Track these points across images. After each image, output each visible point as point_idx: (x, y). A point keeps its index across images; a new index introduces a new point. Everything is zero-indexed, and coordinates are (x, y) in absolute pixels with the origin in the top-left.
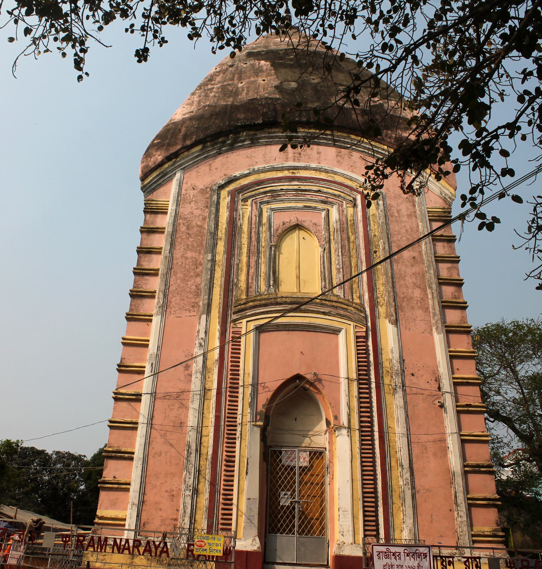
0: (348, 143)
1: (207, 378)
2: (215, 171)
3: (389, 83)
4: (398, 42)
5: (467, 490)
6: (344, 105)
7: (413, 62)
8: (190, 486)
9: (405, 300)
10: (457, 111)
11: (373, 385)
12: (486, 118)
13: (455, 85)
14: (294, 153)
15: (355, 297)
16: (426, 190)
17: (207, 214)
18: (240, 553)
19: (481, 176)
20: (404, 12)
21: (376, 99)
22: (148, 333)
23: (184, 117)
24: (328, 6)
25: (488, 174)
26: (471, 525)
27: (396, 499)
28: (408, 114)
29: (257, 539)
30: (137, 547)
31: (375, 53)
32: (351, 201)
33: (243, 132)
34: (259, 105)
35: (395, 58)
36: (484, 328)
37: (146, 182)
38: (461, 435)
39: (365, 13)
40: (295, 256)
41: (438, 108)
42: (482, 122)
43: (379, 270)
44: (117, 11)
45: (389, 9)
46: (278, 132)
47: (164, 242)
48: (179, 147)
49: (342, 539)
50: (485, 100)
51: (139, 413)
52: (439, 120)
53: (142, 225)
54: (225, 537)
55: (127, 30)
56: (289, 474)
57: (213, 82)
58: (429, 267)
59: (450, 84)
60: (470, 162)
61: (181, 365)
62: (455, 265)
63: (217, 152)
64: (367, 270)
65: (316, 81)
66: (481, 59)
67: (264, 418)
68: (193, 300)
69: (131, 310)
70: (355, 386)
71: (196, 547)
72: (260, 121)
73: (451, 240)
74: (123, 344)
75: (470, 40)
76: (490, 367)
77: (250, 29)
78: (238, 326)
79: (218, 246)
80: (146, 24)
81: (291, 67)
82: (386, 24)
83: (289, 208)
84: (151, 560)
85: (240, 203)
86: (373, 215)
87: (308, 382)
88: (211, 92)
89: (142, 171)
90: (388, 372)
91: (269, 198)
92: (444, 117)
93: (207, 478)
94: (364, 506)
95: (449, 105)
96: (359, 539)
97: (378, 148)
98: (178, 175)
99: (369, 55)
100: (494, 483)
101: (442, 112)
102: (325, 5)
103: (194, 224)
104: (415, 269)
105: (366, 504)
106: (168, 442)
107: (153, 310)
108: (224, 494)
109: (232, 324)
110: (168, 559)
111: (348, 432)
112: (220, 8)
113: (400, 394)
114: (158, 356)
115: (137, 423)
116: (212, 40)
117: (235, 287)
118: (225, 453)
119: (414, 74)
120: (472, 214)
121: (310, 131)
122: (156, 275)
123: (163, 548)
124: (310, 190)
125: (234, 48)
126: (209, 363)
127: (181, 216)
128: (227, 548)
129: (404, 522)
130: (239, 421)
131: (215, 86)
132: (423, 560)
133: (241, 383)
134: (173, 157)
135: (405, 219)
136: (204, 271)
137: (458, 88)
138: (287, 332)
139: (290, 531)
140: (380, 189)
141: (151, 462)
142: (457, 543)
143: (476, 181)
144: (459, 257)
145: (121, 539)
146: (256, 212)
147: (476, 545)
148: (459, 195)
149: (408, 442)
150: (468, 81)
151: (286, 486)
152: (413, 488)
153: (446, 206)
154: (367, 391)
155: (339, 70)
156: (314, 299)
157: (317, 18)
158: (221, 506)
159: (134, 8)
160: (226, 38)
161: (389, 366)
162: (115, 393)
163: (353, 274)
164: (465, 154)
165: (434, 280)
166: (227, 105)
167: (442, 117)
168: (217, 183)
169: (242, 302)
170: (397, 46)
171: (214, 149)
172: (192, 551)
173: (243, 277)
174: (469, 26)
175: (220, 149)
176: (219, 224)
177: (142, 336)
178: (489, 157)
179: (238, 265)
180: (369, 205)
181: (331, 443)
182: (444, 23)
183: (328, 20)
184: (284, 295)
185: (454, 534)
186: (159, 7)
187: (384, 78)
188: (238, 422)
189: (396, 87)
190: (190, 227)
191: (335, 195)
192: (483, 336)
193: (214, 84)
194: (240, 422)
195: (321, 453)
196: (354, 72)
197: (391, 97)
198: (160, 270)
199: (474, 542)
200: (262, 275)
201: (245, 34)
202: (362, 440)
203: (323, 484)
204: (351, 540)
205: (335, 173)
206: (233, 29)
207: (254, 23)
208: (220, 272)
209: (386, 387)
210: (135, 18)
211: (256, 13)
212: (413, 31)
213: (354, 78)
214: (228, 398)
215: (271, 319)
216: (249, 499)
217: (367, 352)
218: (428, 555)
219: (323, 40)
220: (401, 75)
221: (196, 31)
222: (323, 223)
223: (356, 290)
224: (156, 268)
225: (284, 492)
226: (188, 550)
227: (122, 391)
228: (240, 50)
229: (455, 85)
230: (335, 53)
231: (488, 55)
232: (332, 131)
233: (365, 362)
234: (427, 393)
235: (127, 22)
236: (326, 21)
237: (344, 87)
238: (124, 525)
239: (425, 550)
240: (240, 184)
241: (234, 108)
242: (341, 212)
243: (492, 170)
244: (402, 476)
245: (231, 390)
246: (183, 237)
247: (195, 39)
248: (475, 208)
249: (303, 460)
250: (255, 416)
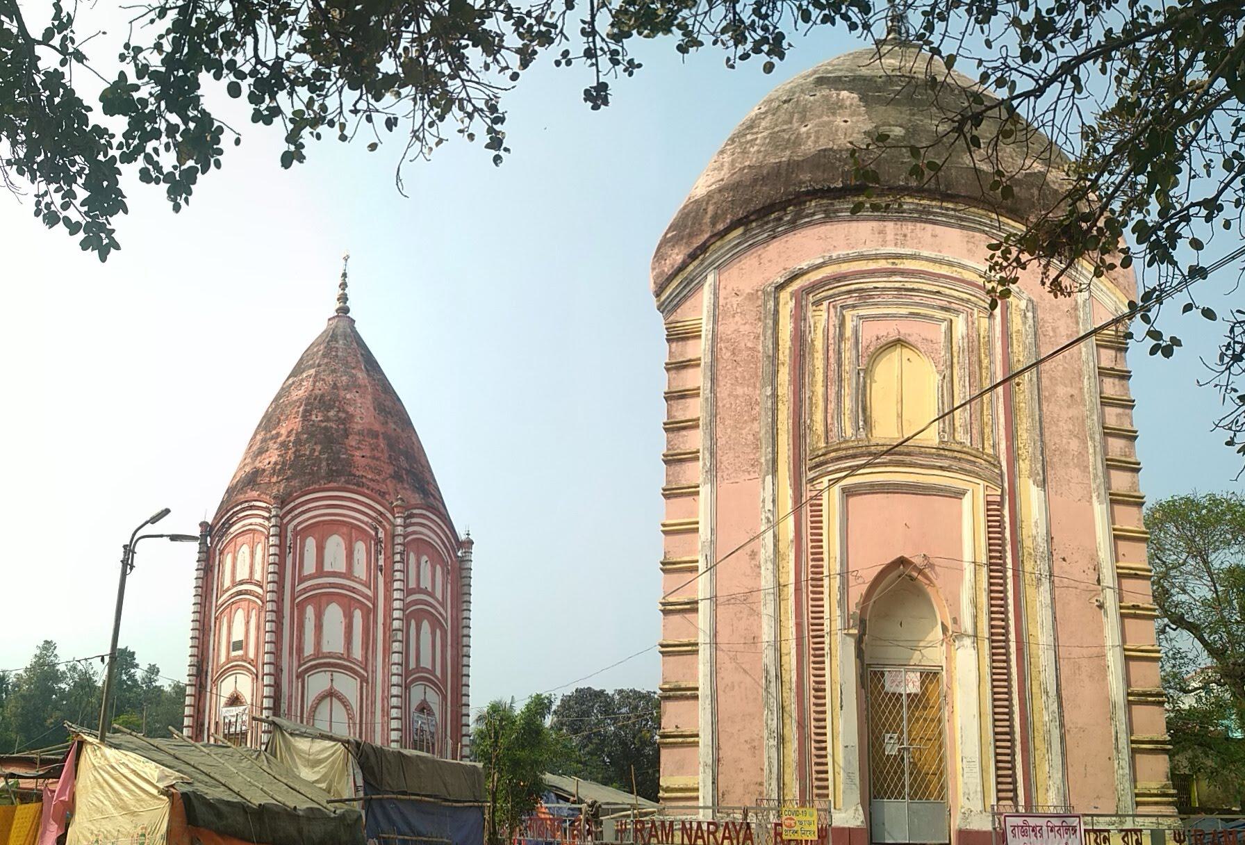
0: (985, 225)
5: (1131, 730)
11: (1010, 573)
14: (896, 234)
15: (986, 446)
17: (760, 331)
18: (841, 830)
22: (694, 512)
26: (1134, 780)
27: (1039, 742)
33: (811, 201)
37: (663, 298)
38: (1125, 650)
40: (895, 385)
48: (706, 236)
49: (968, 805)
51: (697, 628)
53: (667, 361)
57: (755, 130)
69: (668, 482)
71: (784, 828)
74: (664, 532)
83: (886, 316)
85: (810, 307)
87: (915, 568)
90: (1030, 554)
98: (710, 279)
105: (999, 751)
113: (1046, 585)
115: (697, 644)
117: (808, 431)
118: (812, 678)
122: (697, 426)
126: (782, 545)
130: (827, 629)
133: (826, 573)
134: (699, 252)
136: (763, 413)
139: (900, 793)
146: (834, 321)
147: (1142, 810)
152: (1062, 725)
154: (1001, 581)
162: (663, 604)
171: (764, 231)
173: (819, 416)
176: (780, 342)
179: (810, 398)
190: (736, 351)
191: (962, 300)
193: (757, 133)
195: (936, 674)
199: (1138, 804)
200: (847, 412)
202: (994, 654)
203: (940, 721)
204: (980, 807)
205: (964, 267)
208: (786, 412)
217: (1001, 525)
222: (943, 340)
224: (694, 417)
225: (889, 735)
227: (671, 599)
233: (999, 539)
234: (1082, 586)
238: (697, 798)
241: (794, 166)
244: (1047, 708)
245: (814, 583)
249: (912, 685)
250: (847, 618)
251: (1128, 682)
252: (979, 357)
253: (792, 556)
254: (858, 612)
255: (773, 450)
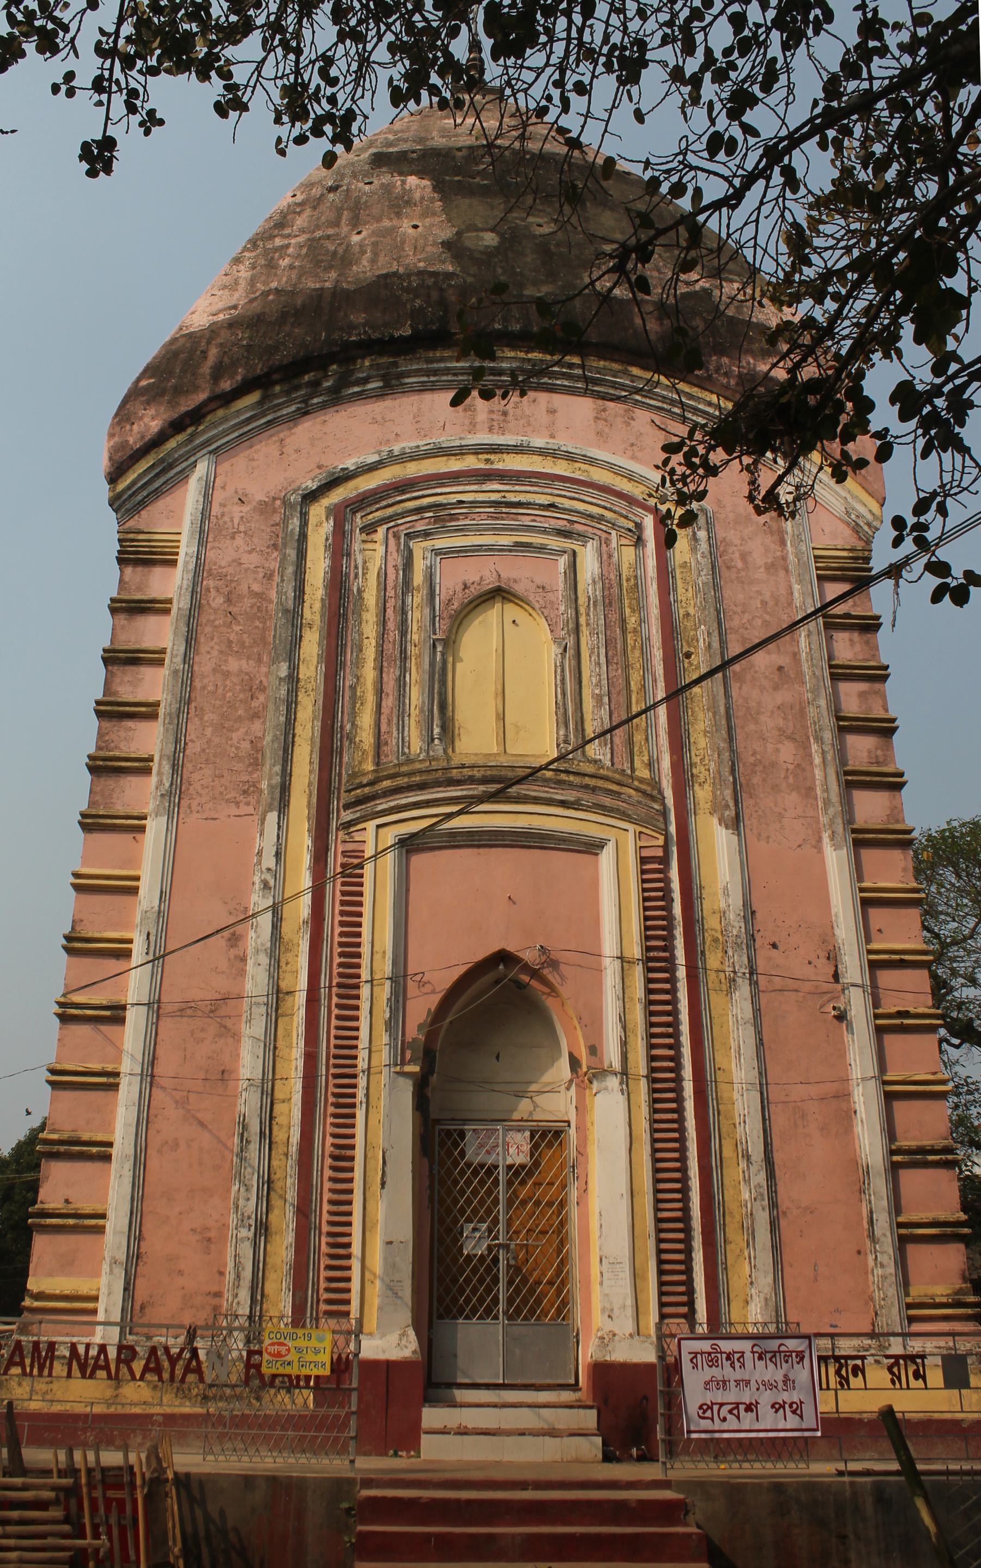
0: (622, 387)
1: (283, 964)
2: (294, 456)
3: (724, 235)
4: (749, 130)
5: (896, 1206)
6: (611, 289)
7: (784, 185)
8: (249, 1218)
9: (759, 768)
10: (888, 310)
11: (681, 973)
12: (959, 329)
13: (886, 244)
14: (492, 412)
15: (637, 764)
16: (810, 502)
17: (275, 565)
18: (371, 1367)
19: (942, 471)
20: (765, 54)
21: (694, 276)
22: (135, 861)
23: (215, 319)
24: (574, 34)
25: (959, 466)
26: (905, 1283)
28: (770, 316)
29: (411, 1333)
30: (128, 1363)
31: (692, 159)
32: (630, 530)
33: (363, 358)
34: (403, 289)
35: (740, 172)
36: (944, 830)
37: (121, 486)
38: (885, 1083)
39: (669, 54)
40: (493, 665)
41: (842, 300)
42: (949, 339)
43: (696, 699)
44: (27, 35)
45: (728, 44)
46: (450, 359)
47: (170, 636)
48: (202, 396)
49: (609, 1326)
50: (958, 283)
51: (120, 1051)
52: (845, 332)
53: (115, 595)
54: (334, 1332)
55: (55, 89)
56: (482, 1183)
57: (287, 231)
58: (815, 690)
59: (873, 244)
60: (916, 437)
61: (219, 935)
62: (877, 686)
63: (298, 409)
64: (667, 699)
65: (546, 230)
66: (952, 179)
67: (421, 1054)
68: (245, 778)
69: (92, 803)
70: (638, 974)
71: (266, 1356)
72: (407, 331)
73: (869, 626)
75: (926, 130)
76: (954, 920)
77: (374, 93)
78: (357, 839)
79: (305, 643)
80: (106, 74)
81: (484, 192)
82: (720, 85)
84: (161, 1389)
86: (684, 565)
87: (526, 968)
88: (281, 257)
89: (111, 459)
90: (716, 940)
91: (429, 524)
92: (857, 325)
93: (289, 1197)
94: (660, 1251)
95: (869, 294)
96: (648, 1323)
97: (698, 399)
98: (202, 468)
99: (675, 164)
100: (956, 1185)
101: (852, 313)
102: (569, 30)
103: (244, 588)
104: (784, 696)
106: (194, 1116)
107: (147, 803)
108: (330, 1234)
109: (341, 833)
110: (201, 1386)
111: (621, 1083)
112: (298, 35)
113: (744, 989)
114: (162, 915)
115: (117, 1074)
116: (278, 121)
117: (346, 743)
118: (330, 1140)
119: (787, 213)
120: (918, 566)
121: (530, 356)
122: (153, 716)
123: (190, 1360)
124: (530, 504)
125: (334, 141)
126: (287, 929)
127: (210, 570)
128: (340, 1356)
129: (752, 1283)
130: (362, 1064)
131: (293, 241)
132: (796, 1365)
133: (365, 974)
134: (188, 421)
135: (761, 574)
136: (271, 707)
137: (893, 252)
138: (476, 850)
140: (699, 500)
141: (153, 1164)
142: (873, 1325)
143: (930, 483)
144: (887, 668)
145: (88, 1346)
146: (396, 559)
147: (916, 1327)
148: (888, 515)
149: (762, 1102)
150: (918, 234)
151: (476, 1212)
152: (773, 1204)
153: (860, 545)
154: (668, 986)
155: (604, 201)
156: (540, 769)
157: (547, 64)
158: (325, 1261)
159: (73, 27)
160: (312, 115)
161: (718, 927)
162: (61, 1004)
163: (635, 709)
164: (904, 417)
165: (828, 722)
166: (322, 289)
167: (854, 325)
168: (299, 488)
169: (365, 781)
170: (746, 139)
171: (290, 402)
172: (258, 1367)
173: (366, 719)
174: (928, 92)
175: (305, 402)
177: (121, 868)
178: (962, 425)
179: (353, 688)
180: (669, 540)
181: (581, 1108)
182: (865, 85)
183: (574, 71)
184: (467, 761)
185: (866, 1304)
186: (135, 26)
187: (713, 224)
188: (359, 1068)
189: (741, 247)
191: (591, 516)
192: (940, 849)
194: (366, 1067)
195: (558, 1133)
196: (641, 206)
197: (731, 272)
198: (162, 705)
199: (911, 1320)
201: (364, 104)
202: (655, 1101)
203: (563, 1204)
204: (629, 1327)
205: (592, 461)
206: (329, 91)
207: (383, 75)
208: (310, 708)
209: (712, 976)
210: (77, 56)
211: (392, 48)
212: (787, 104)
213: (637, 221)
214: (336, 1011)
215: (435, 820)
216: (391, 1243)
218: (807, 1354)
219: (560, 123)
220: (754, 217)
221: (236, 96)
223: (641, 747)
225: (472, 1225)
226: (248, 1365)
227: (78, 998)
228: (348, 146)
229: (886, 244)
230: (590, 158)
231: (967, 170)
232: (583, 356)
234: (808, 987)
235: (56, 67)
236: (568, 73)
237: (615, 246)
238: (94, 1312)
239: (800, 1345)
240: (356, 488)
242: (605, 558)
243: (967, 457)
244: (747, 1181)
245: (342, 991)
246: (217, 623)
247: (233, 115)
248: (927, 551)
251: (890, 1132)
252: (622, 614)
253: (304, 947)
254: (422, 1037)
255: (284, 770)
